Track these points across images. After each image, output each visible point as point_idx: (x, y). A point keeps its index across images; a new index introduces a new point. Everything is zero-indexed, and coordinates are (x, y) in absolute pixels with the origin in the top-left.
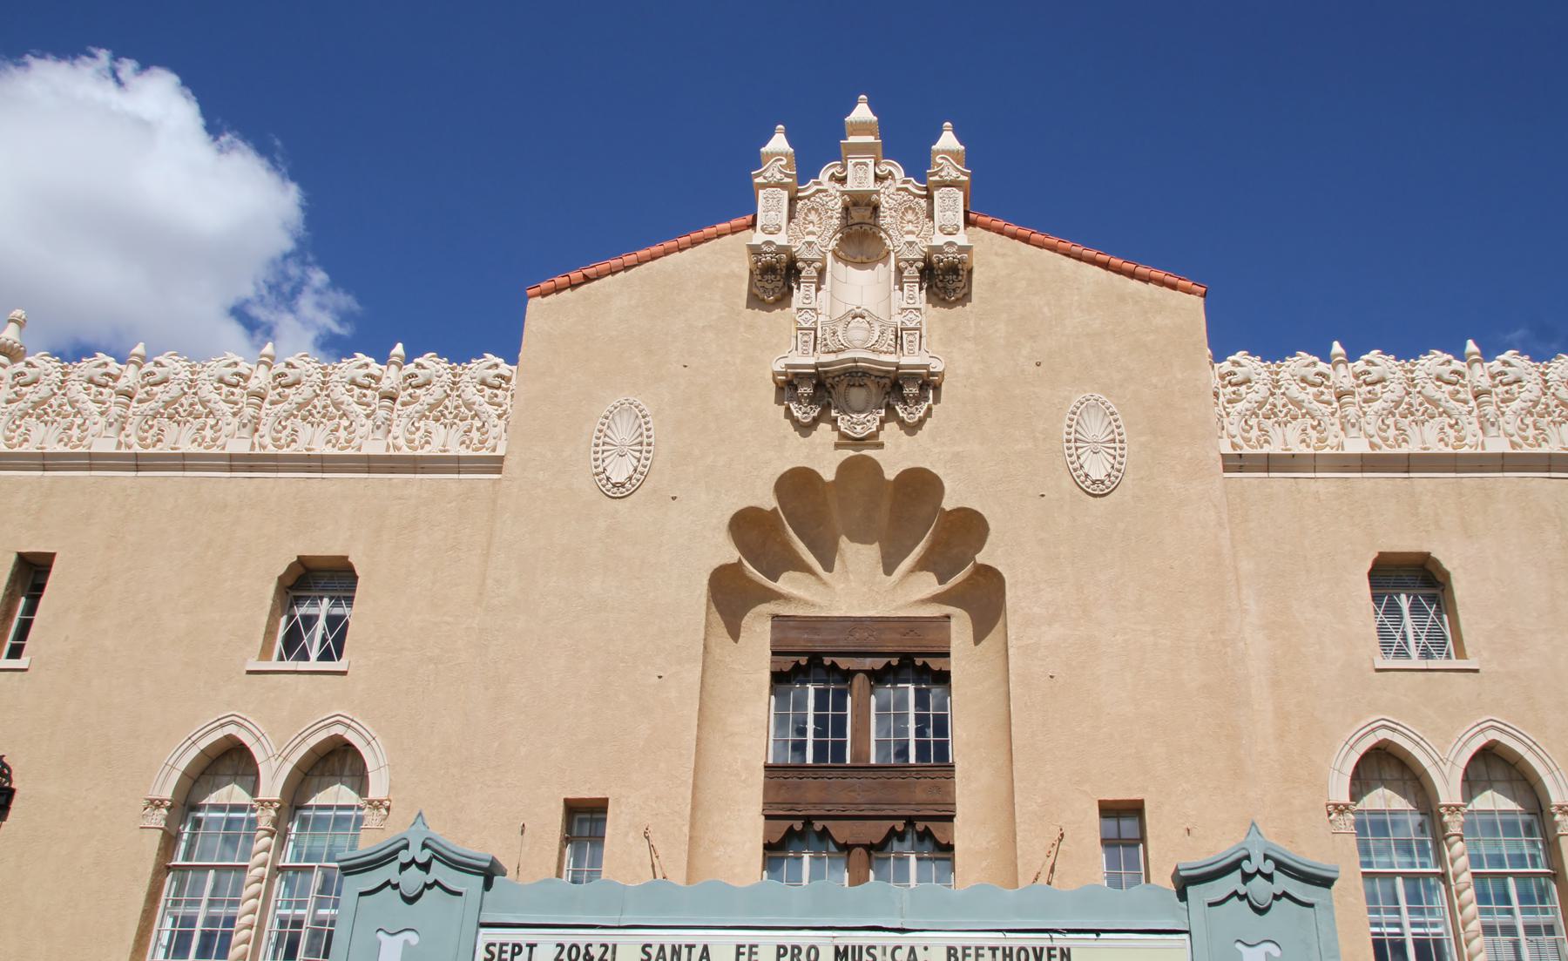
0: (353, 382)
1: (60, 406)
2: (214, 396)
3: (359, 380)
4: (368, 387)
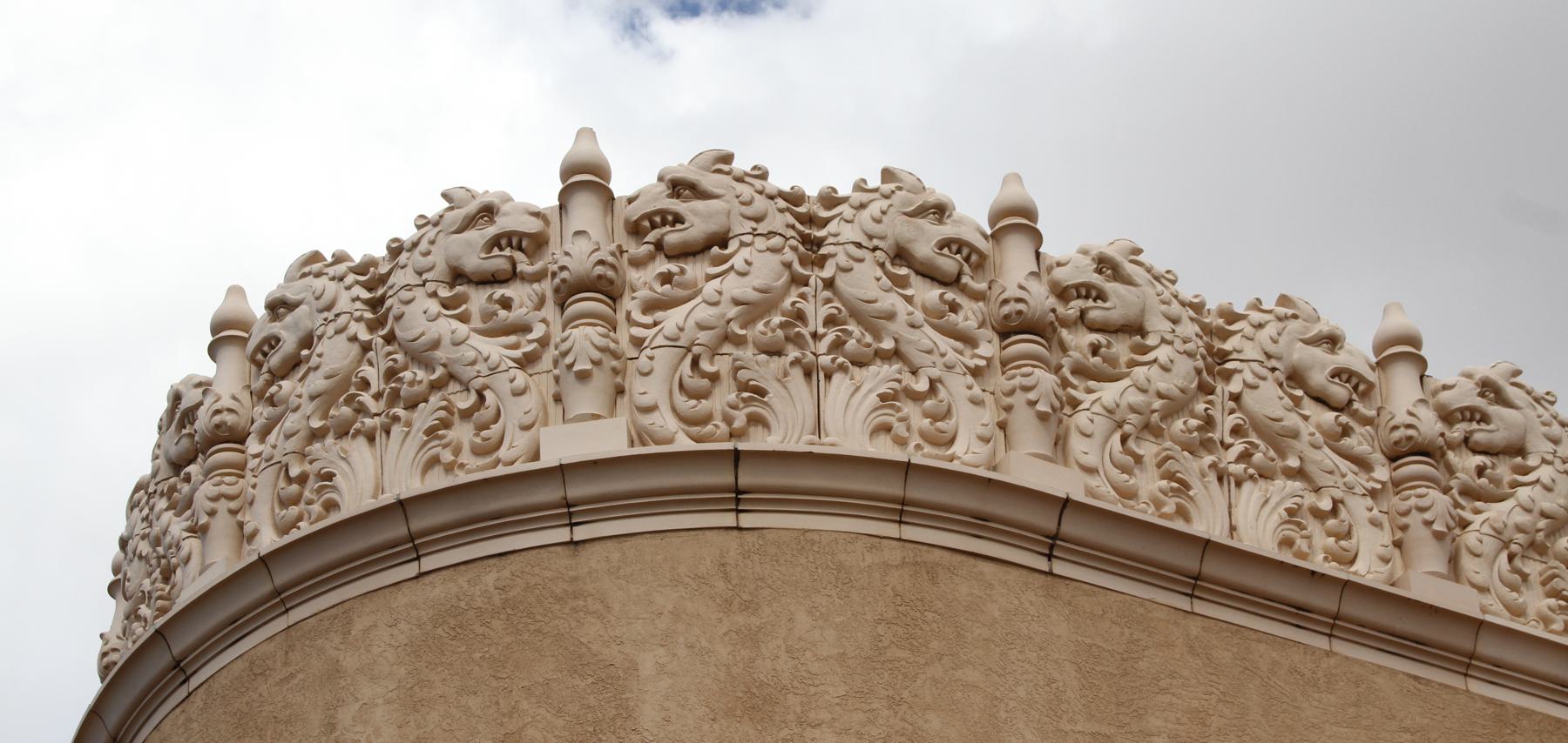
0: (457, 276)
1: (391, 374)
2: (447, 326)
3: (473, 261)
4: (512, 276)
